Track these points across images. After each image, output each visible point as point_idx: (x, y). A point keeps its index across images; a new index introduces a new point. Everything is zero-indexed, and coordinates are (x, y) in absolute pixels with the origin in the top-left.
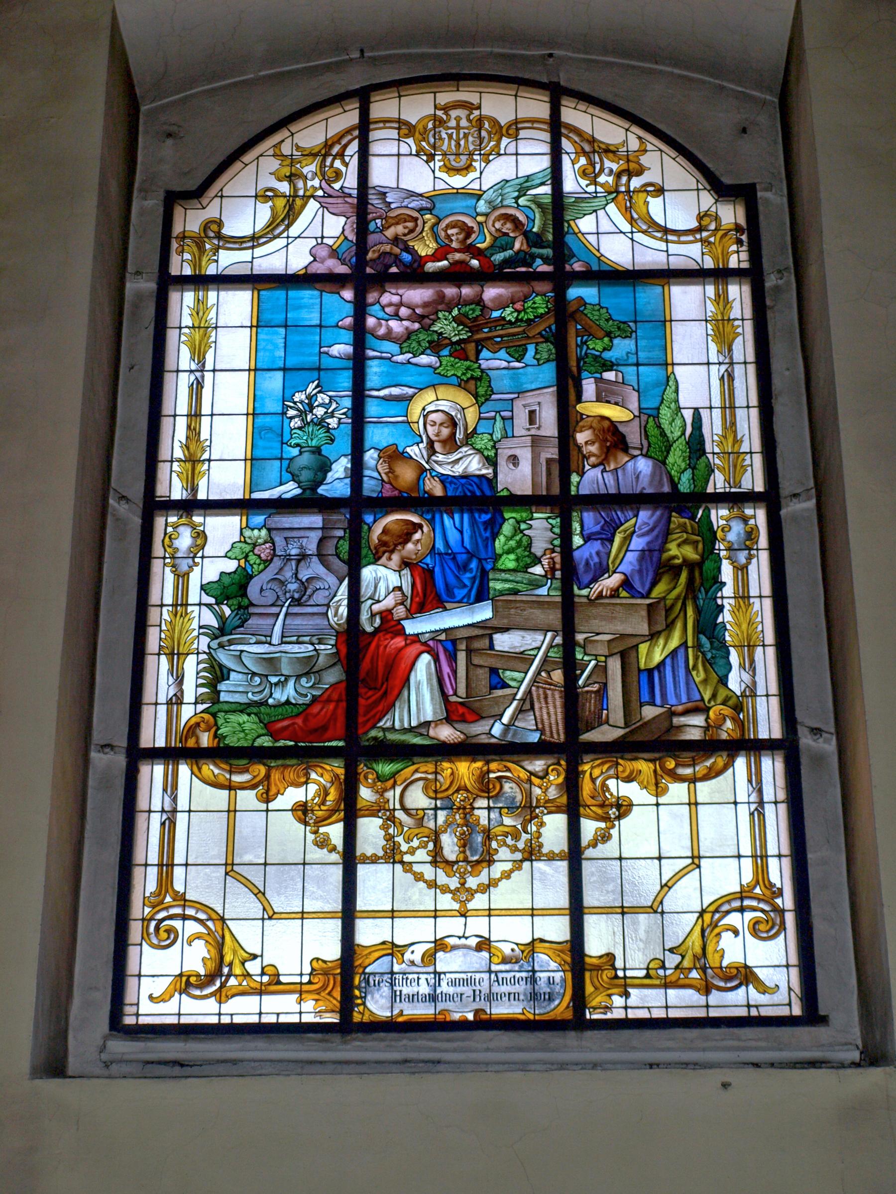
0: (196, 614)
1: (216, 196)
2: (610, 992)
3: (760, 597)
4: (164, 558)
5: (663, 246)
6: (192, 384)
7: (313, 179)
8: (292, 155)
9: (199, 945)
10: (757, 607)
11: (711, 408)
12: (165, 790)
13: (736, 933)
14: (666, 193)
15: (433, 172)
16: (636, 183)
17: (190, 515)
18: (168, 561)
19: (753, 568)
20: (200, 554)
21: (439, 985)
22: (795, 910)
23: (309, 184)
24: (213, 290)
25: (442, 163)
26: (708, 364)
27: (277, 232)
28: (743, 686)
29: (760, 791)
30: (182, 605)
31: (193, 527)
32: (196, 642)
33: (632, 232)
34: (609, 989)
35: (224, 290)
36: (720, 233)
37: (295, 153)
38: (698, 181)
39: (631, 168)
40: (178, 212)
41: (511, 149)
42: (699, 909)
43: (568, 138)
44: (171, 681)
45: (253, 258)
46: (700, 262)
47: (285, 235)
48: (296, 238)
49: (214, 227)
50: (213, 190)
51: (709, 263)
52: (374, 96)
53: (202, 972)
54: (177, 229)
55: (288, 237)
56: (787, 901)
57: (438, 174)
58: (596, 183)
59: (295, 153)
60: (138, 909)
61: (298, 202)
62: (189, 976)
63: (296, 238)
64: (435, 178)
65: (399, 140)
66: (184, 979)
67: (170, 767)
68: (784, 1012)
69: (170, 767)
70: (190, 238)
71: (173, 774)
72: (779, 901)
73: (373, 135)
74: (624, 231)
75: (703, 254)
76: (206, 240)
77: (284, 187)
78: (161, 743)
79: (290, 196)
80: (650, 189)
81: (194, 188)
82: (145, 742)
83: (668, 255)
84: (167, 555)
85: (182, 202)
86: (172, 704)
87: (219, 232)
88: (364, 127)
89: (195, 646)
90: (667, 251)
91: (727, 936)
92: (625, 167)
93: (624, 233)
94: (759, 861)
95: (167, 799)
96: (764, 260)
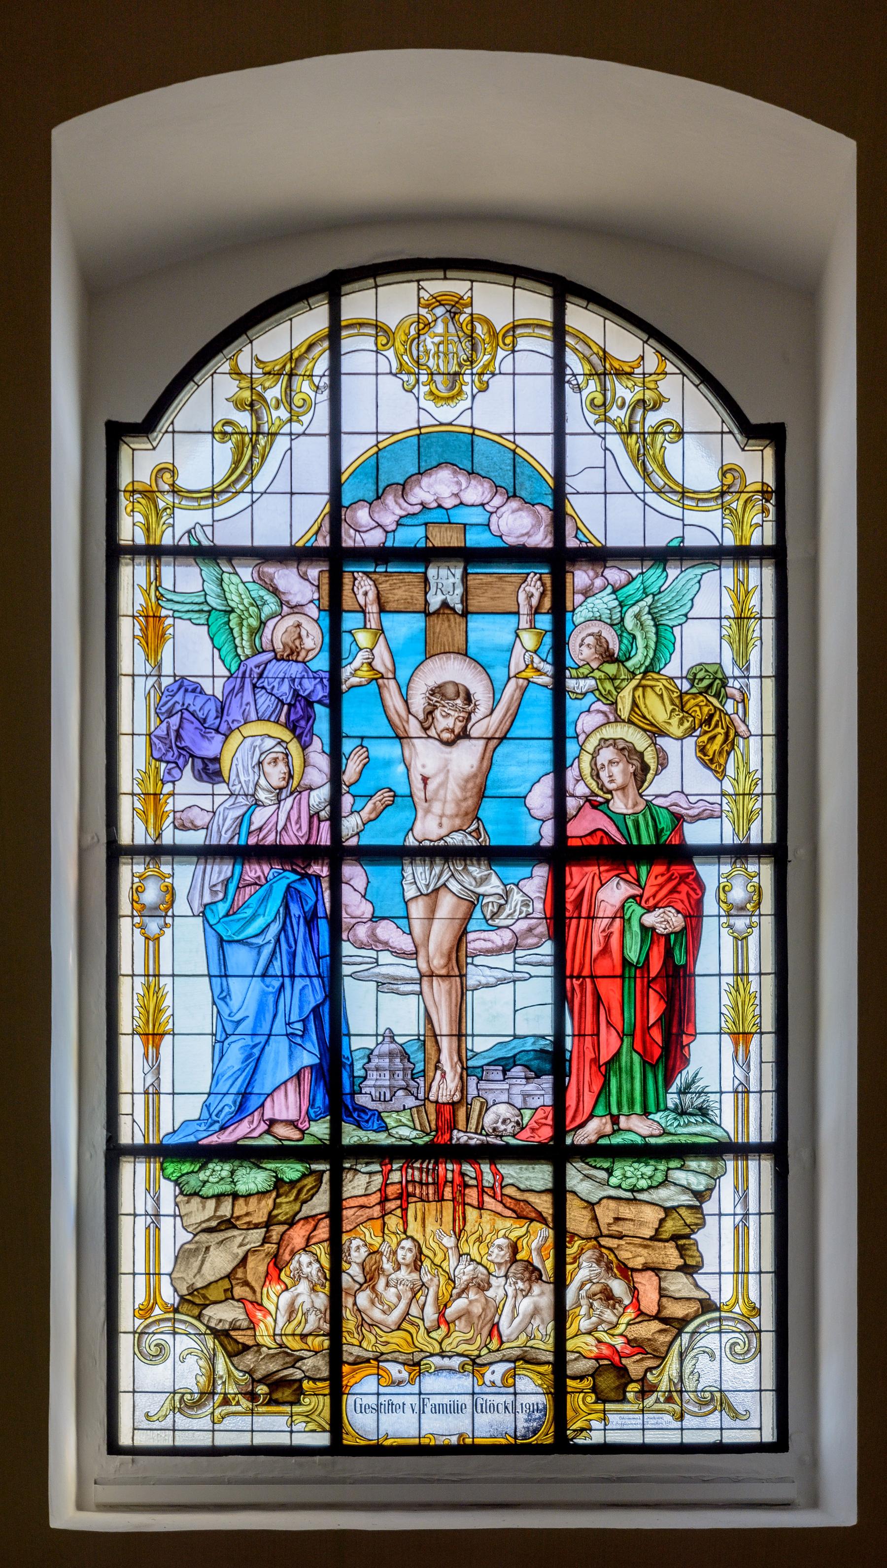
0: (169, 988)
1: (166, 432)
2: (589, 1417)
3: (760, 974)
4: (133, 916)
5: (677, 512)
6: (149, 693)
7: (277, 407)
8: (252, 374)
9: (191, 1360)
10: (754, 987)
11: (720, 1215)
12: (148, 1190)
13: (712, 1356)
14: (686, 436)
15: (418, 399)
16: (653, 419)
17: (158, 864)
18: (137, 920)
19: (753, 941)
20: (170, 913)
21: (424, 1412)
22: (775, 915)
23: (275, 414)
24: (168, 564)
25: (427, 388)
26: (720, 1033)
27: (239, 486)
28: (737, 1082)
29: (746, 1204)
30: (154, 976)
31: (162, 877)
32: (171, 1021)
33: (644, 493)
34: (589, 1414)
35: (180, 863)
36: (744, 496)
37: (255, 370)
38: (723, 422)
39: (647, 397)
40: (125, 453)
41: (507, 367)
42: (681, 376)
43: (575, 350)
44: (147, 1069)
45: (214, 521)
46: (719, 536)
47: (249, 489)
48: (262, 494)
49: (167, 476)
50: (164, 424)
51: (729, 540)
52: (349, 566)
53: (196, 1390)
54: (124, 480)
55: (252, 492)
56: (767, 1320)
57: (423, 403)
58: (606, 420)
59: (255, 370)
60: (127, 1321)
61: (262, 440)
62: (184, 1394)
63: (262, 494)
64: (419, 408)
65: (377, 352)
66: (177, 1397)
67: (152, 1165)
68: (752, 1437)
69: (152, 568)
70: (140, 492)
71: (155, 1247)
72: (756, 1321)
73: (346, 345)
74: (635, 490)
75: (723, 526)
76: (158, 494)
77: (244, 420)
78: (139, 1140)
79: (252, 433)
80: (667, 429)
81: (139, 420)
82: (125, 1139)
83: (684, 525)
84: (135, 913)
85: (127, 439)
86: (148, 1094)
87: (173, 485)
88: (334, 334)
89: (170, 1026)
90: (683, 520)
91: (704, 1359)
92: (640, 396)
93: (636, 494)
94: (740, 943)
95: (150, 1202)
96: (789, 1142)
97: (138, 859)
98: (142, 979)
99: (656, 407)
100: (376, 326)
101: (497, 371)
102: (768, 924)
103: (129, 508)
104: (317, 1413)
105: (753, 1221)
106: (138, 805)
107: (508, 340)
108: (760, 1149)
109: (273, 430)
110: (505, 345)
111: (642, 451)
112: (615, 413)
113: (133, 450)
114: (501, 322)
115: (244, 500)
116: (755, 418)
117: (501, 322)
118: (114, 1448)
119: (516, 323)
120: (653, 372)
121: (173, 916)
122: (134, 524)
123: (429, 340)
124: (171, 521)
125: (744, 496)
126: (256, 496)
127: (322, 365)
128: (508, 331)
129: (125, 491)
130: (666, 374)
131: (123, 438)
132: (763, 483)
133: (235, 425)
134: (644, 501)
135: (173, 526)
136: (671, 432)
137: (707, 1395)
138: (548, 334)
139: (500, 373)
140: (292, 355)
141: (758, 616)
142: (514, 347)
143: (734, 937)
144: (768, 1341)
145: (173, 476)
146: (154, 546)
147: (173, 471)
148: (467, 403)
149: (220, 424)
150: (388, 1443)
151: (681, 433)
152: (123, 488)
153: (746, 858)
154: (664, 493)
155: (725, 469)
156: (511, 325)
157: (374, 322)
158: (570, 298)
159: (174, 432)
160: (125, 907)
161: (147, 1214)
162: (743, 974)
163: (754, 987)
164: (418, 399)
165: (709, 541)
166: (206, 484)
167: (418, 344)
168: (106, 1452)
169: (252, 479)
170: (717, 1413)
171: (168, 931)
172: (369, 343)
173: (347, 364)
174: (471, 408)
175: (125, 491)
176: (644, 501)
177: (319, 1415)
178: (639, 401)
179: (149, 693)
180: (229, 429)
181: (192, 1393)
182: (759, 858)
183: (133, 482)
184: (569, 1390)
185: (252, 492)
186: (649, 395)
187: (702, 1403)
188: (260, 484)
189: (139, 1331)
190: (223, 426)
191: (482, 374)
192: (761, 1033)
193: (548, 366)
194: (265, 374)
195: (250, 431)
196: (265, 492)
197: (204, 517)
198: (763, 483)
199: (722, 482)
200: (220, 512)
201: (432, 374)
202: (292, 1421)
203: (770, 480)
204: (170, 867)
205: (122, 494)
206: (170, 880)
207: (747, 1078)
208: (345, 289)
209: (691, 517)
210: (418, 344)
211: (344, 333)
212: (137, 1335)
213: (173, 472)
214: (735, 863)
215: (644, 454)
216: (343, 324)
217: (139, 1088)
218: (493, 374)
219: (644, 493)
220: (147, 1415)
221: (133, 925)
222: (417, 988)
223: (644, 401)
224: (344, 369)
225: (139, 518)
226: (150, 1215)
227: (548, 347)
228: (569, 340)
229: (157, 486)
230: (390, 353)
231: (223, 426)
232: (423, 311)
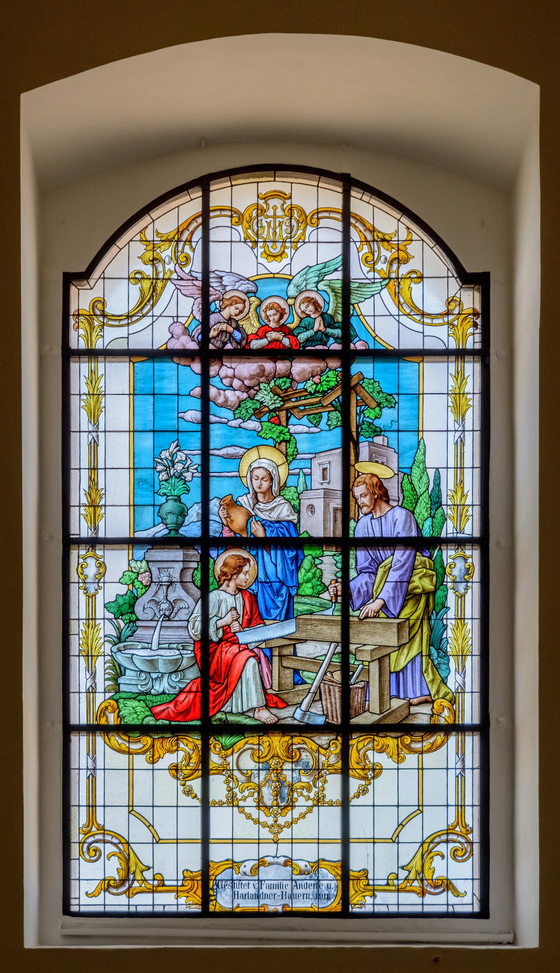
2: (364, 894)
4: (79, 583)
5: (419, 327)
6: (91, 443)
9: (114, 859)
12: (88, 754)
13: (443, 857)
15: (257, 257)
16: (404, 270)
19: (468, 597)
27: (145, 311)
28: (457, 685)
33: (399, 315)
36: (462, 317)
38: (448, 269)
40: (73, 290)
42: (421, 242)
47: (150, 314)
49: (100, 306)
50: (96, 274)
51: (453, 345)
54: (73, 309)
55: (153, 316)
56: (475, 837)
57: (261, 260)
60: (75, 836)
61: (160, 284)
62: (109, 880)
66: (106, 882)
68: (468, 909)
72: (470, 836)
73: (213, 223)
74: (393, 314)
75: (448, 335)
76: (94, 317)
77: (148, 270)
79: (153, 279)
80: (414, 275)
83: (424, 336)
84: (80, 581)
87: (103, 311)
89: (102, 650)
90: (423, 333)
91: (437, 859)
93: (393, 316)
95: (90, 761)
97: (82, 547)
98: (84, 621)
99: (406, 261)
100: (231, 210)
101: (307, 240)
102: (477, 587)
103: (76, 325)
104: (193, 891)
105: (468, 773)
106: (83, 512)
107: (314, 221)
108: (472, 728)
109: (166, 276)
110: (312, 224)
111: (397, 290)
112: (379, 266)
113: (79, 289)
114: (309, 208)
115: (147, 321)
116: (469, 269)
117: (309, 208)
118: (66, 910)
119: (319, 210)
120: (404, 239)
121: (104, 583)
122: (79, 336)
123: (264, 221)
124: (102, 333)
125: (462, 317)
126: (155, 318)
127: (198, 235)
128: (313, 215)
129: (73, 315)
130: (412, 241)
131: (73, 282)
132: (474, 309)
133: (141, 273)
134: (398, 321)
135: (103, 337)
136: (416, 278)
137: (440, 882)
138: (339, 216)
139: (309, 242)
140: (178, 230)
141: (103, 393)
142: (318, 225)
143: (456, 595)
144: (476, 848)
145: (103, 305)
146: (92, 350)
147: (104, 303)
148: (287, 261)
149: (133, 274)
150: (238, 910)
151: (421, 278)
152: (72, 314)
153: (465, 546)
154: (411, 315)
155: (454, 298)
156: (316, 211)
157: (230, 208)
158: (354, 188)
159: (104, 278)
160: (74, 577)
161: (88, 769)
162: (461, 619)
163: (469, 627)
164: (257, 257)
165: (440, 346)
166: (124, 311)
167: (258, 222)
168: (62, 913)
169: (153, 306)
170: (445, 893)
171: (101, 592)
172: (227, 221)
173: (214, 235)
174: (290, 264)
175: (73, 315)
176: (398, 321)
177: (195, 893)
178: (395, 259)
179: (91, 443)
180: (138, 276)
181: (115, 880)
182: (472, 546)
183: (79, 310)
184: (351, 878)
185: (153, 316)
186: (402, 254)
187: (436, 887)
188: (157, 311)
189: (82, 841)
190: (135, 274)
191: (298, 242)
192: (472, 655)
193: (339, 237)
194: (163, 241)
195: (152, 277)
196: (161, 316)
197: (123, 332)
198: (474, 309)
199: (448, 308)
200: (134, 328)
201: (265, 242)
202: (178, 897)
203: (478, 308)
204: (102, 552)
205: (71, 317)
206: (102, 560)
207: (464, 683)
208: (211, 182)
209: (429, 330)
210: (258, 222)
211: (212, 214)
212: (81, 845)
213: (104, 303)
214: (458, 549)
215: (399, 292)
216: (211, 209)
217: (83, 689)
218: (305, 242)
219: (399, 315)
220: (87, 894)
221: (79, 588)
222: (231, 866)
223: (398, 258)
224: (212, 238)
225: (82, 332)
226: (90, 769)
227: (339, 225)
228: (352, 221)
229: (93, 312)
230: (239, 228)
231: (135, 274)
232: (261, 202)
